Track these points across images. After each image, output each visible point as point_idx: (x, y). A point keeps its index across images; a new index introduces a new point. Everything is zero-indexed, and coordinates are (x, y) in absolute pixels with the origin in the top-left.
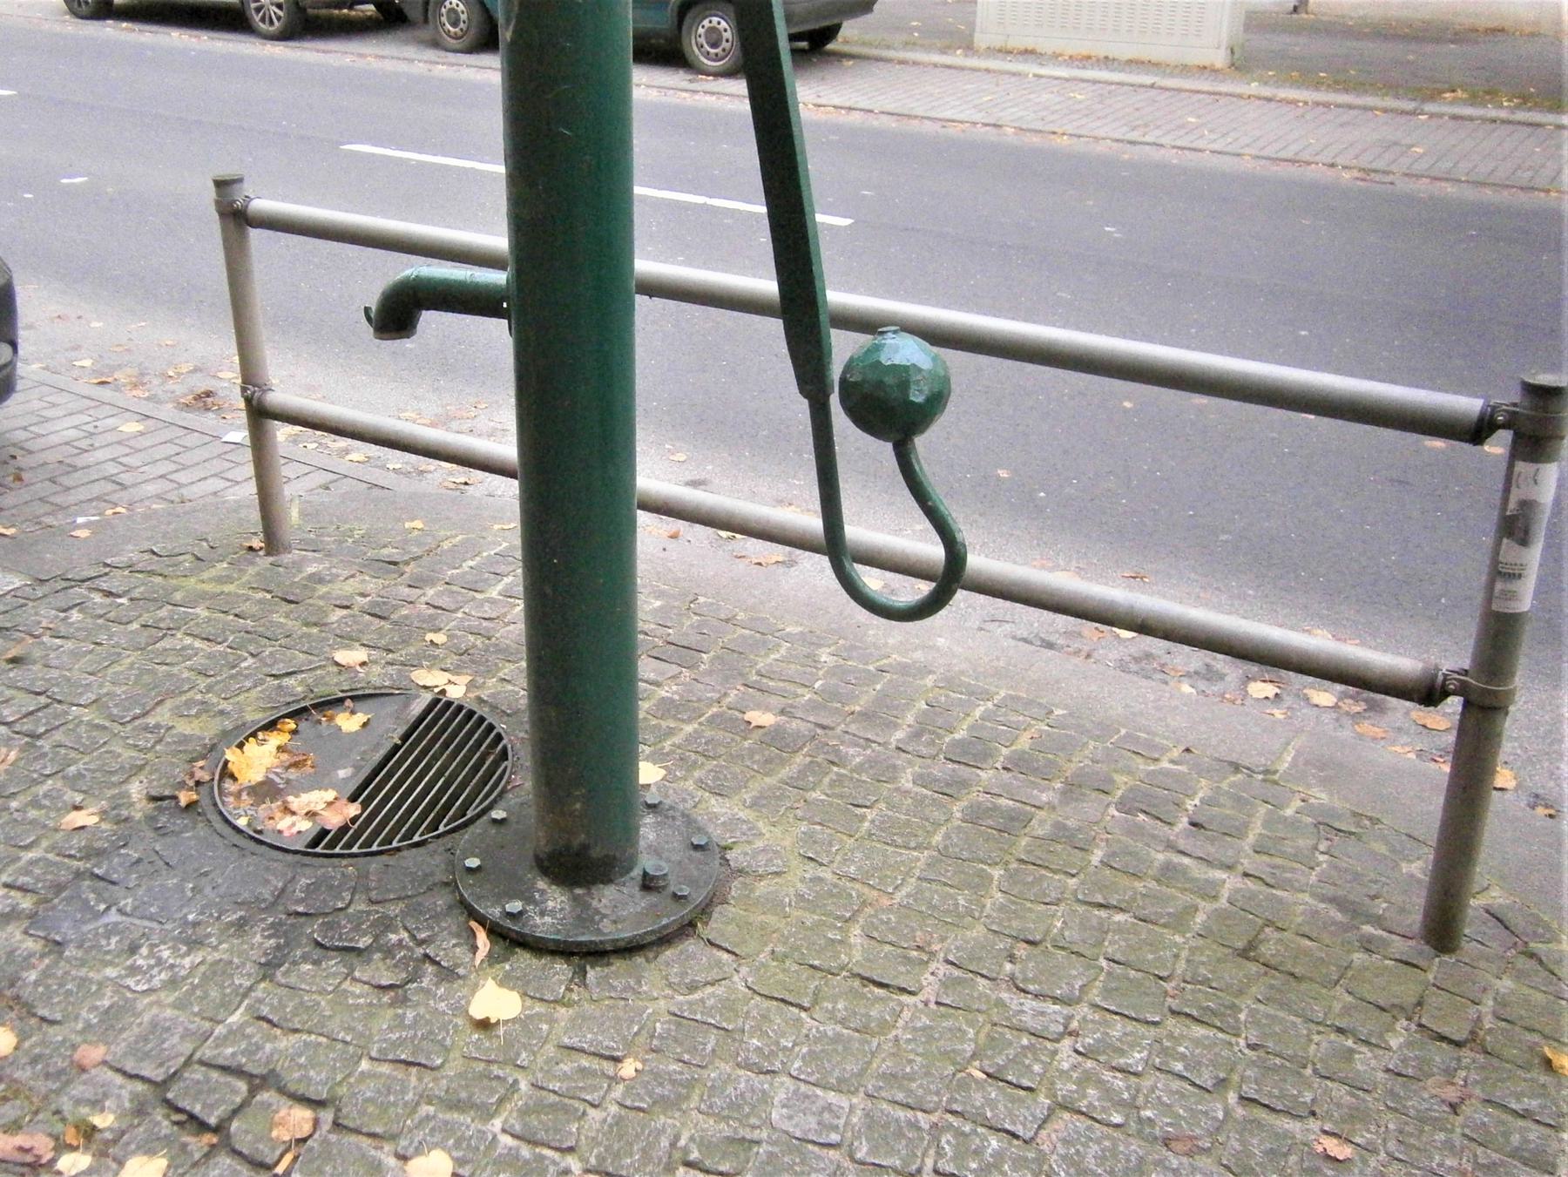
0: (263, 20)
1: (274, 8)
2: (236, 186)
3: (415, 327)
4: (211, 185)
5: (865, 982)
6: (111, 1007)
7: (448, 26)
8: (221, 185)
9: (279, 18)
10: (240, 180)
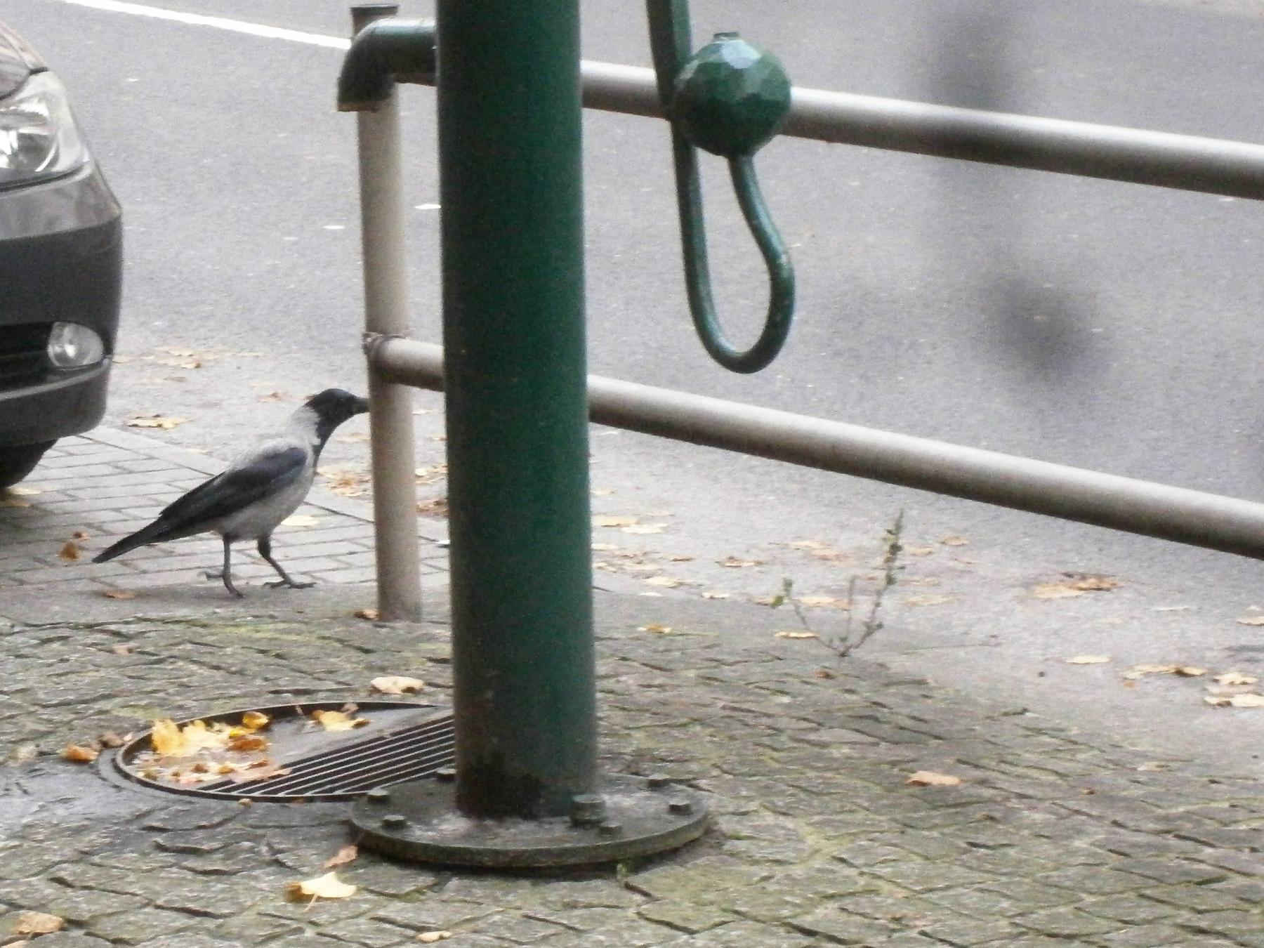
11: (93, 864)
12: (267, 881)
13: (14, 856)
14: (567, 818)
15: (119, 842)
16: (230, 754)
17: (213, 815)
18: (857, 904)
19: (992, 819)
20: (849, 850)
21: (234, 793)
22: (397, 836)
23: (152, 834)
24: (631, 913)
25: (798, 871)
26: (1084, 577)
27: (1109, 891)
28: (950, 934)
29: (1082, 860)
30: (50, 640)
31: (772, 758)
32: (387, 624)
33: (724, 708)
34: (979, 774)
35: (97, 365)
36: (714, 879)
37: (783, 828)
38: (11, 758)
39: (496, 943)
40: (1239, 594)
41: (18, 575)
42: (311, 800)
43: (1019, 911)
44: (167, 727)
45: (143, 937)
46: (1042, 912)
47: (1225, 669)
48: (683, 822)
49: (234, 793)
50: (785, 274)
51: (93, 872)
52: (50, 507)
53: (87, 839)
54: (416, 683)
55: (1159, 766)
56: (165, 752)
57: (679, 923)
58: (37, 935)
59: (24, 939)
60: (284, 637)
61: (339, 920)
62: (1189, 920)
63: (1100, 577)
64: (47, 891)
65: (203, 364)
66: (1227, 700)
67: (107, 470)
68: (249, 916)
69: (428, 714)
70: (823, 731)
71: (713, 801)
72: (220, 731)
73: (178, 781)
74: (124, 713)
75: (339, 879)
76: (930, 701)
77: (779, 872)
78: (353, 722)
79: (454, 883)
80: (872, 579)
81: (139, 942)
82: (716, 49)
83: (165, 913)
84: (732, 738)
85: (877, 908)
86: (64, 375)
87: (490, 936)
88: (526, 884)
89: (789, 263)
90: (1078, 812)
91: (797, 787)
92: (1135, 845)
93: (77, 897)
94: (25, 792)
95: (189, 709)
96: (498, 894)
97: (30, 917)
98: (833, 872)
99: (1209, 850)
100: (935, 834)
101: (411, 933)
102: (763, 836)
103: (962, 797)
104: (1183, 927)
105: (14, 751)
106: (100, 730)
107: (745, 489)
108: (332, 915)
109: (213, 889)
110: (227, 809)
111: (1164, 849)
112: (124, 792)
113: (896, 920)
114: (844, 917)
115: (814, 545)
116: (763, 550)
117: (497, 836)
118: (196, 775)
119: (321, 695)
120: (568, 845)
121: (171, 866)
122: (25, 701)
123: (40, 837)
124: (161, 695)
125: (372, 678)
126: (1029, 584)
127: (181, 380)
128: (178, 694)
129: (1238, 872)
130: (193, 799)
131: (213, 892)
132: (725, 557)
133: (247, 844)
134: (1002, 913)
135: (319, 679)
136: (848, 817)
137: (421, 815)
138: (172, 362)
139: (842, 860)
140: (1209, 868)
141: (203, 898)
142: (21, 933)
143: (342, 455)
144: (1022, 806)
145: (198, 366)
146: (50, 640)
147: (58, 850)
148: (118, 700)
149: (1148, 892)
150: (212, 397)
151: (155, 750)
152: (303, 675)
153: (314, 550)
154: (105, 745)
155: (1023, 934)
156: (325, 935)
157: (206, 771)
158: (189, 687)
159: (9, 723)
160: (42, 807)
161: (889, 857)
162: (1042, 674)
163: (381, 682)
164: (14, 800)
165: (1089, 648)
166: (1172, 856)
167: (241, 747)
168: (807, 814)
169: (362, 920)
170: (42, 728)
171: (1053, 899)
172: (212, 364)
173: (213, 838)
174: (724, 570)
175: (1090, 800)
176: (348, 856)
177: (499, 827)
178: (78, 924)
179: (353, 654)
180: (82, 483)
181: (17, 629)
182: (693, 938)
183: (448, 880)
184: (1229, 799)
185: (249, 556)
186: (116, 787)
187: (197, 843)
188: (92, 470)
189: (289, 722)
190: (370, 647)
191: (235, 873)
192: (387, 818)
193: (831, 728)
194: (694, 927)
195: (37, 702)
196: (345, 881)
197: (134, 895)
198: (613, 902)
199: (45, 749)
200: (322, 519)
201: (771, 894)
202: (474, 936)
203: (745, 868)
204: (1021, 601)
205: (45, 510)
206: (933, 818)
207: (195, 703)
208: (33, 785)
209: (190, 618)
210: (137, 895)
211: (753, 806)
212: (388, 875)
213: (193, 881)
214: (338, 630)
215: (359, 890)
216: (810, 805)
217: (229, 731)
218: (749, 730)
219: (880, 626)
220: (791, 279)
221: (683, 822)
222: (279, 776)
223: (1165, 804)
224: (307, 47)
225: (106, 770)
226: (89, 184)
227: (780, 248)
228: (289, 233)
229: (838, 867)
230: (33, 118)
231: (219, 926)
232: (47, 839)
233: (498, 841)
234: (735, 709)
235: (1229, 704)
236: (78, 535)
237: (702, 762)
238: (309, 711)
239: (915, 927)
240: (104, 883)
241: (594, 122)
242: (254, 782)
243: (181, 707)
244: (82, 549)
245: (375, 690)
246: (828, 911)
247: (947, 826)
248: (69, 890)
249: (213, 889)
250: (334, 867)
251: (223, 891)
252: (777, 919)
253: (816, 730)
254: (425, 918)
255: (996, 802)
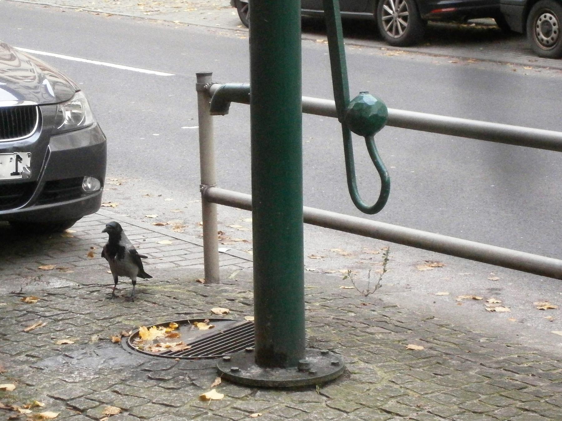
0: (390, 30)
1: (400, 20)
2: (207, 77)
3: (228, 109)
4: (196, 76)
5: (382, 411)
6: (56, 384)
7: (542, 36)
8: (200, 76)
9: (403, 28)
10: (210, 74)
11: (127, 385)
12: (191, 392)
13: (98, 381)
14: (296, 368)
15: (135, 376)
16: (167, 339)
17: (167, 365)
18: (403, 400)
19: (439, 363)
20: (395, 377)
21: (173, 356)
22: (237, 375)
23: (145, 372)
24: (324, 404)
25: (379, 386)
26: (432, 262)
27: (489, 393)
28: (439, 412)
29: (475, 380)
30: (93, 292)
31: (357, 340)
32: (208, 285)
33: (333, 318)
34: (429, 345)
35: (99, 190)
36: (350, 390)
37: (369, 369)
38: (90, 341)
39: (279, 418)
40: (485, 269)
41: (74, 263)
42: (200, 358)
43: (460, 402)
44: (144, 329)
45: (151, 416)
46: (468, 402)
47: (489, 297)
48: (337, 369)
49: (173, 356)
50: (387, 179)
51: (128, 388)
52: (80, 237)
53: (123, 374)
54: (227, 310)
55: (487, 340)
56: (145, 338)
57: (342, 409)
58: (112, 415)
59: (107, 417)
60: (175, 290)
61: (220, 408)
62: (521, 405)
63: (438, 262)
64: (113, 396)
65: (122, 183)
66: (494, 309)
67: (97, 223)
68: (187, 407)
69: (234, 323)
70: (371, 328)
71: (344, 359)
72: (162, 330)
73: (151, 351)
74: (127, 323)
75: (217, 391)
76: (401, 314)
77: (372, 387)
78: (209, 326)
79: (259, 393)
80: (362, 263)
81: (149, 418)
82: (361, 98)
83: (156, 406)
84: (341, 331)
85: (410, 401)
86: (88, 194)
87: (276, 415)
88: (284, 393)
89: (388, 175)
90: (467, 360)
91: (369, 351)
92: (492, 374)
93: (124, 399)
94: (97, 355)
95: (150, 321)
96: (275, 397)
97: (108, 408)
98: (391, 387)
99: (517, 375)
100: (421, 370)
101: (247, 414)
102: (364, 372)
103: (426, 354)
104: (520, 408)
105: (90, 338)
106: (121, 330)
107: (311, 230)
108: (217, 406)
109: (172, 396)
110: (171, 362)
111: (502, 375)
112: (133, 355)
113: (418, 407)
114: (399, 405)
115: (339, 250)
116: (322, 252)
117: (272, 375)
118: (157, 348)
119: (194, 315)
120: (299, 379)
121: (155, 386)
122: (91, 318)
123: (106, 374)
124: (138, 315)
125: (212, 307)
126: (415, 265)
127: (115, 189)
128: (144, 314)
129: (532, 385)
130: (158, 358)
131: (173, 397)
132: (310, 255)
133: (181, 377)
134: (454, 403)
135: (191, 308)
136: (390, 363)
137: (244, 367)
138: (111, 183)
139: (393, 382)
140: (520, 383)
141: (169, 399)
142: (106, 414)
143: (174, 217)
144: (448, 358)
145: (120, 184)
146: (93, 292)
147: (114, 379)
148: (123, 317)
149: (503, 394)
150: (127, 195)
151: (140, 338)
152: (185, 306)
153: (174, 253)
154: (123, 336)
155: (464, 412)
156: (216, 415)
157: (161, 347)
158: (147, 312)
159: (87, 327)
160: (104, 361)
161: (409, 380)
162: (434, 302)
163: (215, 310)
164: (93, 358)
165: (442, 289)
166: (506, 378)
167: (172, 336)
168: (376, 362)
169: (228, 408)
170: (100, 329)
171: (471, 397)
172: (125, 183)
173: (168, 374)
174: (311, 260)
175: (470, 355)
176: (218, 382)
177: (272, 371)
178: (126, 410)
179: (200, 297)
180: (90, 228)
181: (81, 287)
182: (348, 415)
183: (256, 392)
184: (517, 354)
185: (151, 255)
186: (130, 353)
187: (163, 377)
188: (92, 223)
189: (185, 326)
190: (206, 294)
191: (179, 389)
192: (232, 368)
193: (373, 326)
194: (348, 411)
195: (95, 318)
196: (219, 392)
197: (144, 398)
198: (316, 400)
199: (102, 338)
200: (173, 241)
201: (372, 396)
202: (270, 415)
203: (360, 386)
204: (414, 271)
205: (78, 238)
206: (420, 363)
207: (151, 319)
208: (99, 352)
209: (140, 283)
210: (145, 398)
211: (356, 359)
212: (234, 388)
213: (164, 392)
214: (191, 288)
215: (225, 396)
216: (376, 359)
217: (165, 330)
218: (346, 328)
219: (381, 286)
220: (389, 181)
221: (337, 369)
222: (187, 349)
223: (495, 356)
224: (136, 72)
225: (125, 346)
226: (95, 129)
227: (385, 170)
228: (141, 137)
229: (392, 384)
230: (78, 107)
231: (178, 411)
232: (108, 374)
233: (273, 377)
234: (338, 319)
235: (495, 311)
236: (92, 248)
237: (334, 342)
238: (193, 322)
239: (426, 409)
240: (132, 393)
241: (307, 119)
242: (179, 351)
243: (146, 320)
244: (94, 253)
245: (213, 313)
246: (392, 403)
247: (426, 366)
248: (120, 395)
249: (172, 396)
250: (214, 386)
251: (176, 397)
252: (376, 407)
253: (367, 327)
254: (251, 408)
255: (439, 356)
